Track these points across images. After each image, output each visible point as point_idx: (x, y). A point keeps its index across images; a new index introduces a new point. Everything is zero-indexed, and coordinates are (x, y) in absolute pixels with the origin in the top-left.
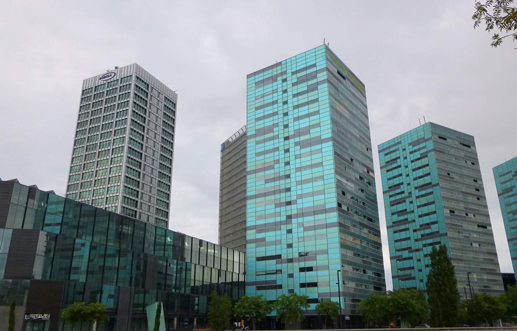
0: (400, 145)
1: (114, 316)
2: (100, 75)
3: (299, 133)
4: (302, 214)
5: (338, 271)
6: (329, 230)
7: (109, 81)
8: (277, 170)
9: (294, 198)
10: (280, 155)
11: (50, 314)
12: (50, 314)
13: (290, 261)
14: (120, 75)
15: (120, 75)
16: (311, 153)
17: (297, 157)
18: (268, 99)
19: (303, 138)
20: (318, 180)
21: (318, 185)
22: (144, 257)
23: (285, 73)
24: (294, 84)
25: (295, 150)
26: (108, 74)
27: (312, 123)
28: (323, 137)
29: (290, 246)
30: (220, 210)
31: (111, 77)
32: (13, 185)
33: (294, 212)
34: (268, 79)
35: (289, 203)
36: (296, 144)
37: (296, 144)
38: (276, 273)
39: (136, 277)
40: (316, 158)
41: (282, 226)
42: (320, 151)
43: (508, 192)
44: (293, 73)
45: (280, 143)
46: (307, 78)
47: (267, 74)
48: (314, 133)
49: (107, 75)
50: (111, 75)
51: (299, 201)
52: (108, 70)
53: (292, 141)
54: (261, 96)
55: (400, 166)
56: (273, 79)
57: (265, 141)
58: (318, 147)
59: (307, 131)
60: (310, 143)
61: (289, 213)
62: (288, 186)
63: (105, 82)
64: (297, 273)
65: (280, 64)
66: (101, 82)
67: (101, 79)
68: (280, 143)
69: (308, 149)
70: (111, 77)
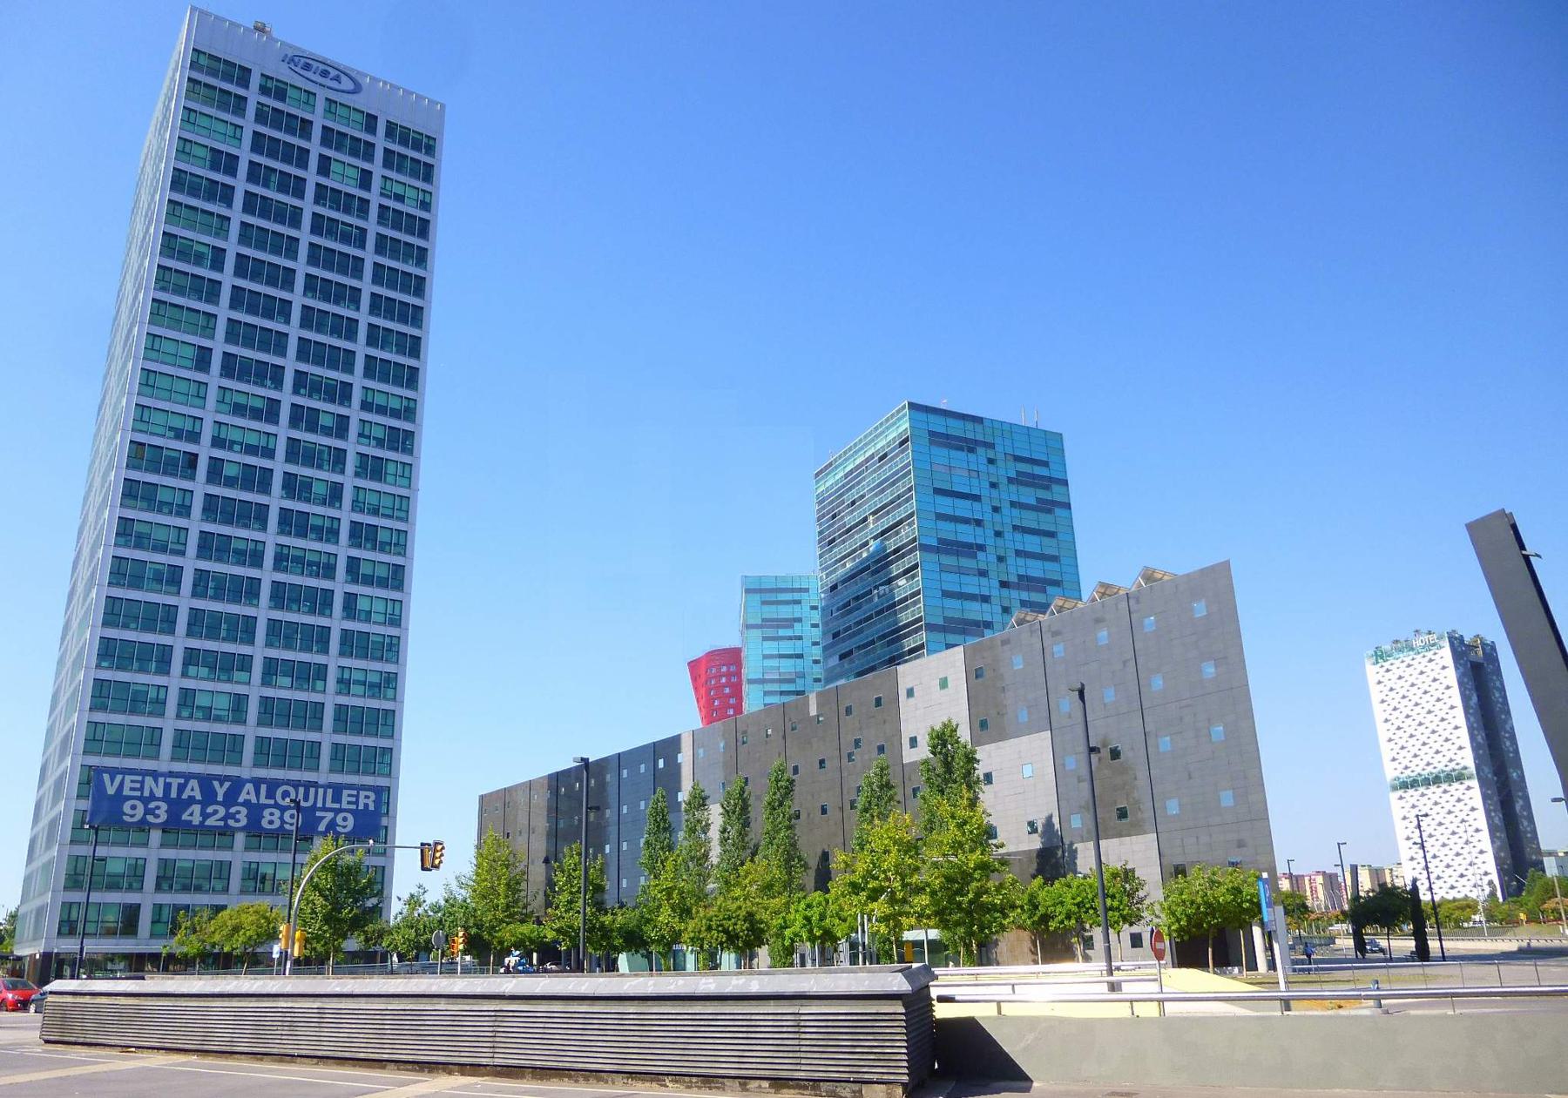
0: (804, 596)
23: (991, 446)
47: (956, 428)
50: (337, 79)
53: (1014, 594)
55: (800, 638)
56: (970, 446)
66: (284, 73)
70: (334, 84)
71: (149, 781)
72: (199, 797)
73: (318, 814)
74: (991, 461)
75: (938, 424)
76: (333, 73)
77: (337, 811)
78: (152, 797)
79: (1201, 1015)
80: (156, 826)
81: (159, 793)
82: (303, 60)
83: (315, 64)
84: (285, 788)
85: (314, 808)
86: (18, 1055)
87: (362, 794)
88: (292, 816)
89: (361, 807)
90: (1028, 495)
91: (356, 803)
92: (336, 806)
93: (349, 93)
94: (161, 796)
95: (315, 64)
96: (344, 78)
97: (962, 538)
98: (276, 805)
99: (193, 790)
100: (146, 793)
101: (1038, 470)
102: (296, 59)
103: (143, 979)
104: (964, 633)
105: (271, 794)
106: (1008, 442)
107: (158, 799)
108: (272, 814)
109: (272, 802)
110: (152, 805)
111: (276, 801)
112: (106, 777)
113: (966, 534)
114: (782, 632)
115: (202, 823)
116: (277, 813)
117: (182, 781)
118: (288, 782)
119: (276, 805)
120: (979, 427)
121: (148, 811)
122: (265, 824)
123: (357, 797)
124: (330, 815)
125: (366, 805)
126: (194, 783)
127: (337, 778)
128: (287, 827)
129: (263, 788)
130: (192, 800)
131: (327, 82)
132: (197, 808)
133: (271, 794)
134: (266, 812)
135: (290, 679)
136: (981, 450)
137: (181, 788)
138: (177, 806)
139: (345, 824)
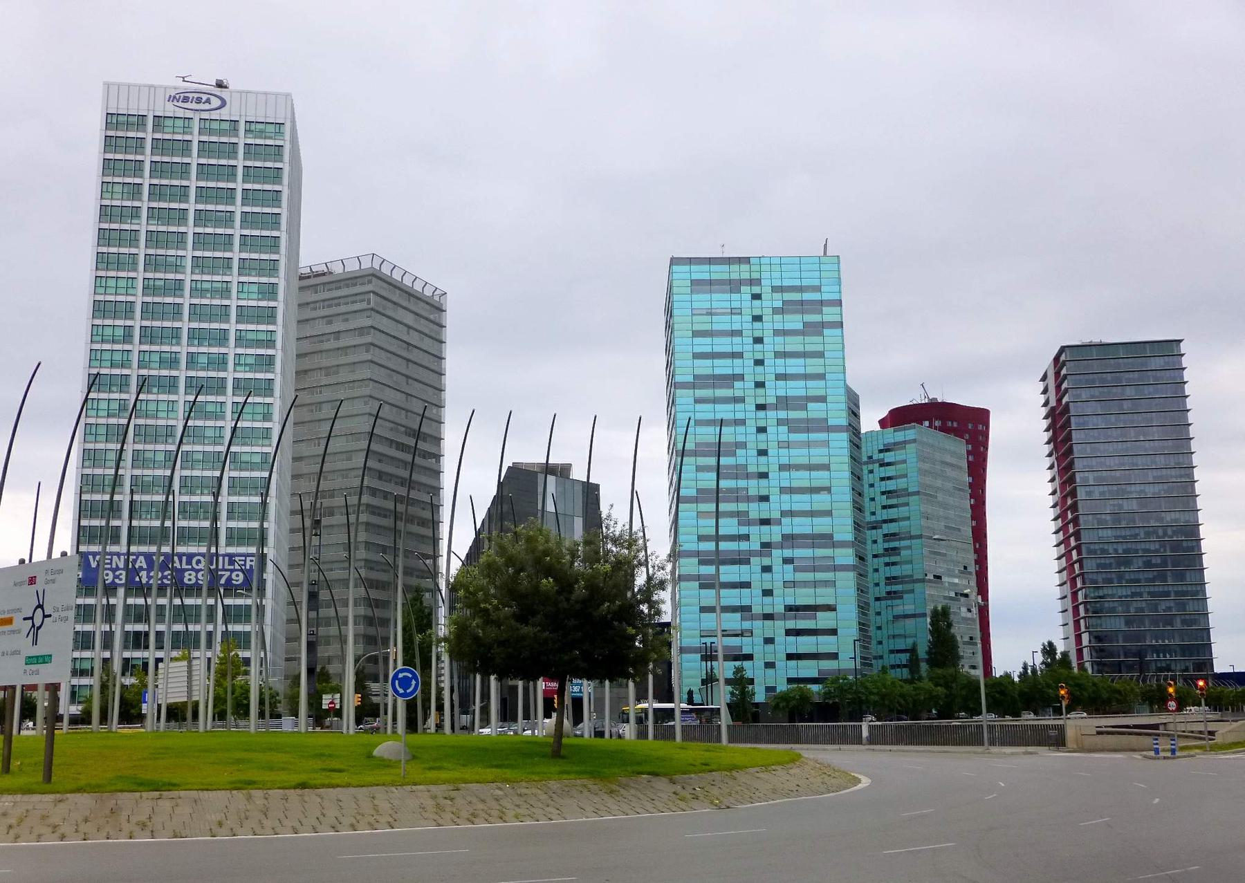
1: (267, 732)
2: (171, 88)
3: (784, 402)
4: (790, 540)
5: (855, 641)
6: (913, 541)
7: (205, 115)
8: (741, 461)
9: (776, 515)
10: (744, 344)
13: (768, 617)
14: (244, 102)
15: (244, 102)
16: (808, 444)
17: (788, 445)
18: (722, 323)
19: (794, 415)
20: (822, 492)
21: (821, 501)
23: (758, 282)
24: (776, 311)
25: (777, 433)
27: (811, 393)
28: (831, 422)
29: (768, 593)
31: (207, 106)
33: (777, 538)
34: (721, 282)
35: (765, 522)
36: (780, 422)
37: (780, 422)
38: (742, 635)
40: (818, 456)
41: (743, 288)
42: (826, 444)
44: (775, 289)
45: (746, 411)
46: (801, 307)
47: (719, 272)
48: (815, 410)
49: (196, 95)
50: (208, 101)
51: (785, 521)
52: (183, 78)
53: (771, 414)
54: (704, 312)
56: (734, 286)
57: (714, 401)
58: (822, 436)
59: (802, 402)
60: (810, 426)
61: (766, 539)
62: (764, 492)
63: (189, 114)
64: (780, 638)
65: (747, 260)
66: (170, 109)
67: (172, 99)
68: (746, 411)
69: (802, 437)
70: (207, 106)
71: (115, 558)
72: (145, 566)
73: (220, 573)
74: (756, 297)
75: (701, 272)
76: (204, 97)
77: (232, 571)
78: (118, 568)
79: (499, 705)
80: (121, 585)
81: (121, 565)
82: (182, 95)
83: (190, 95)
84: (236, 573)
85: (217, 569)
86: (1231, 679)
87: (248, 559)
88: (203, 575)
89: (248, 567)
90: (794, 321)
91: (245, 565)
92: (232, 567)
93: (217, 109)
94: (122, 567)
95: (190, 95)
96: (212, 98)
97: (718, 371)
98: (193, 569)
99: (141, 563)
100: (114, 566)
101: (807, 296)
102: (177, 96)
103: (1059, 741)
104: (804, 357)
105: (189, 562)
106: (776, 275)
107: (121, 569)
108: (190, 575)
109: (190, 567)
110: (117, 573)
111: (192, 567)
112: (91, 557)
113: (724, 367)
114: (720, 393)
115: (148, 582)
116: (194, 574)
117: (135, 557)
118: (199, 554)
119: (193, 569)
120: (745, 267)
121: (116, 577)
122: (186, 581)
123: (245, 561)
124: (228, 573)
125: (251, 566)
126: (142, 558)
127: (231, 550)
128: (200, 582)
129: (184, 558)
130: (141, 568)
131: (201, 106)
132: (144, 574)
133: (189, 562)
134: (186, 574)
135: (145, 456)
136: (745, 289)
137: (135, 561)
138: (132, 572)
139: (237, 579)
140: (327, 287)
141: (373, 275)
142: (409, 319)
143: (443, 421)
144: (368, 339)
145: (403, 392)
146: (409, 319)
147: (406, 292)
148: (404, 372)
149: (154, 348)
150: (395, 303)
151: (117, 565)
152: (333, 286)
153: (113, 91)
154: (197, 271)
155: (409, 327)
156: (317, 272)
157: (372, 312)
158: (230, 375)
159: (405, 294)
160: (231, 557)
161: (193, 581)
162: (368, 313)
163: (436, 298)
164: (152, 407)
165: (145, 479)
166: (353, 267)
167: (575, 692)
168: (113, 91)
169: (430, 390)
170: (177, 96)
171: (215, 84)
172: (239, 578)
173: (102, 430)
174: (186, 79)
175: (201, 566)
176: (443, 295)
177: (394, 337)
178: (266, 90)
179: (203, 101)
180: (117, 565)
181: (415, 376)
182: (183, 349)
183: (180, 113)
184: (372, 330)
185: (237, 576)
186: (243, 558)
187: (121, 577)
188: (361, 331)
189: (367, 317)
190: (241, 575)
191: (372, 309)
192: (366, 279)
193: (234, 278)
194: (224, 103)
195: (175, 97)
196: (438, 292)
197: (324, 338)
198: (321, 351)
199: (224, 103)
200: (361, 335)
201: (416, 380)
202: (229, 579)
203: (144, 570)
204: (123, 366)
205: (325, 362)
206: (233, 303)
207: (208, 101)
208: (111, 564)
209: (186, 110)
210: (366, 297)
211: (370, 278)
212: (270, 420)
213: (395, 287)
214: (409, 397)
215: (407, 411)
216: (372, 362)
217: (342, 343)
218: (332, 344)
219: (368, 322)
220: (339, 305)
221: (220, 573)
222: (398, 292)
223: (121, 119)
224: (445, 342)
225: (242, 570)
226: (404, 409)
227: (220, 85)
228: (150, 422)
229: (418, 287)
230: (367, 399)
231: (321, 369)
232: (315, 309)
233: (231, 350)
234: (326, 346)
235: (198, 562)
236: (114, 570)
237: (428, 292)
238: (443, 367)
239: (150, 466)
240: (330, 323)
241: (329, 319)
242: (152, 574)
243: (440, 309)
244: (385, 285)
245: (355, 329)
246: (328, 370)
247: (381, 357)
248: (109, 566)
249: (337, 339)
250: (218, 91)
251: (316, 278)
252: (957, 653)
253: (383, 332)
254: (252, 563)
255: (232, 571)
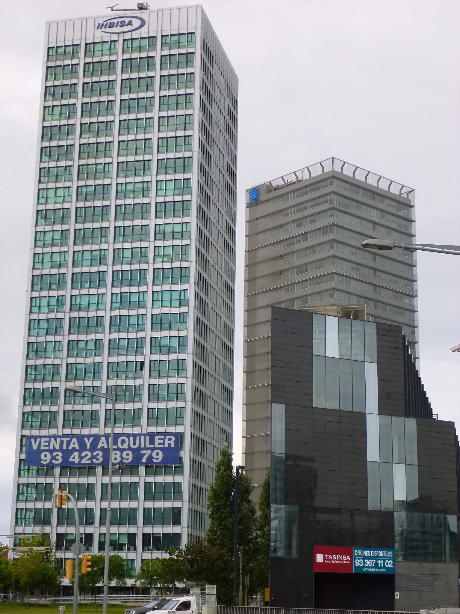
7: (128, 36)
11: (392, 566)
12: (392, 566)
22: (201, 582)
26: (112, 21)
30: (246, 251)
31: (129, 28)
32: (103, 588)
39: (267, 485)
43: (36, 494)
49: (120, 20)
50: (130, 23)
52: (112, 8)
63: (114, 37)
66: (99, 35)
67: (100, 26)
70: (129, 28)
71: (52, 440)
72: (77, 447)
73: (142, 452)
76: (127, 20)
77: (152, 450)
78: (54, 450)
81: (57, 447)
82: (109, 22)
83: (115, 21)
85: (139, 448)
87: (167, 437)
89: (167, 446)
92: (152, 446)
98: (118, 449)
99: (75, 444)
110: (54, 454)
111: (118, 446)
115: (79, 462)
116: (119, 453)
117: (68, 439)
118: (124, 435)
119: (118, 449)
121: (53, 458)
123: (164, 439)
124: (149, 452)
125: (170, 444)
126: (74, 440)
130: (74, 450)
132: (76, 454)
137: (69, 443)
138: (67, 453)
139: (157, 457)
140: (297, 193)
141: (334, 177)
142: (374, 216)
143: (416, 310)
144: (330, 236)
145: (371, 284)
146: (374, 216)
147: (370, 191)
148: (371, 265)
149: (87, 247)
150: (358, 202)
151: (54, 447)
152: (301, 192)
153: (54, 27)
154: (122, 175)
155: (374, 223)
156: (291, 182)
157: (334, 211)
158: (150, 266)
159: (369, 193)
160: (152, 437)
161: (119, 460)
162: (330, 212)
163: (405, 196)
164: (85, 300)
165: (79, 366)
166: (317, 172)
167: (368, 567)
168: (54, 27)
169: (402, 282)
170: (105, 23)
171: (137, 8)
172: (159, 457)
173: (43, 325)
174: (114, 8)
175: (125, 446)
176: (412, 191)
177: (358, 233)
178: (179, 5)
179: (126, 24)
180: (54, 447)
181: (382, 268)
182: (110, 246)
183: (107, 38)
184: (335, 228)
185: (157, 454)
186: (163, 437)
187: (57, 458)
188: (326, 229)
189: (330, 216)
190: (161, 453)
191: (334, 209)
192: (327, 183)
193: (153, 177)
194: (143, 23)
195: (102, 25)
196: (404, 190)
197: (295, 240)
198: (293, 252)
199: (143, 23)
200: (325, 233)
201: (383, 272)
202: (150, 458)
203: (77, 450)
204: (60, 266)
205: (297, 262)
206: (152, 200)
207: (130, 23)
208: (49, 446)
209: (112, 35)
210: (328, 198)
211: (331, 180)
212: (186, 305)
213: (358, 187)
214: (377, 288)
215: (376, 301)
216: (334, 256)
217: (311, 242)
218: (303, 244)
219: (331, 221)
220: (306, 208)
221: (142, 452)
222: (361, 191)
223: (61, 50)
224: (415, 236)
225: (130, 448)
226: (371, 300)
227: (141, 8)
228: (83, 314)
229: (383, 186)
230: (332, 292)
231: (293, 268)
232: (287, 215)
233: (150, 244)
234: (297, 247)
235: (123, 442)
236: (51, 452)
237: (395, 190)
238: (414, 259)
239: (83, 355)
240: (299, 225)
241: (298, 222)
242: (83, 454)
243: (408, 206)
244: (348, 186)
245: (320, 229)
246: (303, 268)
247: (345, 253)
248: (47, 448)
249: (306, 239)
250: (138, 14)
251: (287, 187)
252: (175, 443)
253: (346, 229)
254: (170, 442)
255: (152, 450)
